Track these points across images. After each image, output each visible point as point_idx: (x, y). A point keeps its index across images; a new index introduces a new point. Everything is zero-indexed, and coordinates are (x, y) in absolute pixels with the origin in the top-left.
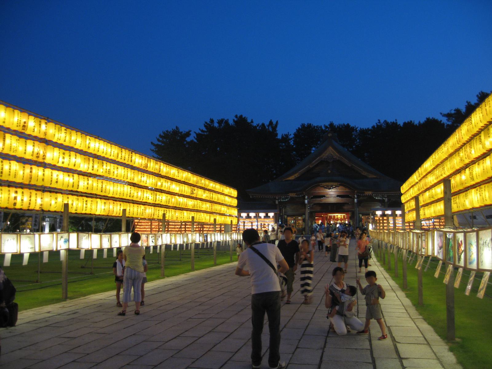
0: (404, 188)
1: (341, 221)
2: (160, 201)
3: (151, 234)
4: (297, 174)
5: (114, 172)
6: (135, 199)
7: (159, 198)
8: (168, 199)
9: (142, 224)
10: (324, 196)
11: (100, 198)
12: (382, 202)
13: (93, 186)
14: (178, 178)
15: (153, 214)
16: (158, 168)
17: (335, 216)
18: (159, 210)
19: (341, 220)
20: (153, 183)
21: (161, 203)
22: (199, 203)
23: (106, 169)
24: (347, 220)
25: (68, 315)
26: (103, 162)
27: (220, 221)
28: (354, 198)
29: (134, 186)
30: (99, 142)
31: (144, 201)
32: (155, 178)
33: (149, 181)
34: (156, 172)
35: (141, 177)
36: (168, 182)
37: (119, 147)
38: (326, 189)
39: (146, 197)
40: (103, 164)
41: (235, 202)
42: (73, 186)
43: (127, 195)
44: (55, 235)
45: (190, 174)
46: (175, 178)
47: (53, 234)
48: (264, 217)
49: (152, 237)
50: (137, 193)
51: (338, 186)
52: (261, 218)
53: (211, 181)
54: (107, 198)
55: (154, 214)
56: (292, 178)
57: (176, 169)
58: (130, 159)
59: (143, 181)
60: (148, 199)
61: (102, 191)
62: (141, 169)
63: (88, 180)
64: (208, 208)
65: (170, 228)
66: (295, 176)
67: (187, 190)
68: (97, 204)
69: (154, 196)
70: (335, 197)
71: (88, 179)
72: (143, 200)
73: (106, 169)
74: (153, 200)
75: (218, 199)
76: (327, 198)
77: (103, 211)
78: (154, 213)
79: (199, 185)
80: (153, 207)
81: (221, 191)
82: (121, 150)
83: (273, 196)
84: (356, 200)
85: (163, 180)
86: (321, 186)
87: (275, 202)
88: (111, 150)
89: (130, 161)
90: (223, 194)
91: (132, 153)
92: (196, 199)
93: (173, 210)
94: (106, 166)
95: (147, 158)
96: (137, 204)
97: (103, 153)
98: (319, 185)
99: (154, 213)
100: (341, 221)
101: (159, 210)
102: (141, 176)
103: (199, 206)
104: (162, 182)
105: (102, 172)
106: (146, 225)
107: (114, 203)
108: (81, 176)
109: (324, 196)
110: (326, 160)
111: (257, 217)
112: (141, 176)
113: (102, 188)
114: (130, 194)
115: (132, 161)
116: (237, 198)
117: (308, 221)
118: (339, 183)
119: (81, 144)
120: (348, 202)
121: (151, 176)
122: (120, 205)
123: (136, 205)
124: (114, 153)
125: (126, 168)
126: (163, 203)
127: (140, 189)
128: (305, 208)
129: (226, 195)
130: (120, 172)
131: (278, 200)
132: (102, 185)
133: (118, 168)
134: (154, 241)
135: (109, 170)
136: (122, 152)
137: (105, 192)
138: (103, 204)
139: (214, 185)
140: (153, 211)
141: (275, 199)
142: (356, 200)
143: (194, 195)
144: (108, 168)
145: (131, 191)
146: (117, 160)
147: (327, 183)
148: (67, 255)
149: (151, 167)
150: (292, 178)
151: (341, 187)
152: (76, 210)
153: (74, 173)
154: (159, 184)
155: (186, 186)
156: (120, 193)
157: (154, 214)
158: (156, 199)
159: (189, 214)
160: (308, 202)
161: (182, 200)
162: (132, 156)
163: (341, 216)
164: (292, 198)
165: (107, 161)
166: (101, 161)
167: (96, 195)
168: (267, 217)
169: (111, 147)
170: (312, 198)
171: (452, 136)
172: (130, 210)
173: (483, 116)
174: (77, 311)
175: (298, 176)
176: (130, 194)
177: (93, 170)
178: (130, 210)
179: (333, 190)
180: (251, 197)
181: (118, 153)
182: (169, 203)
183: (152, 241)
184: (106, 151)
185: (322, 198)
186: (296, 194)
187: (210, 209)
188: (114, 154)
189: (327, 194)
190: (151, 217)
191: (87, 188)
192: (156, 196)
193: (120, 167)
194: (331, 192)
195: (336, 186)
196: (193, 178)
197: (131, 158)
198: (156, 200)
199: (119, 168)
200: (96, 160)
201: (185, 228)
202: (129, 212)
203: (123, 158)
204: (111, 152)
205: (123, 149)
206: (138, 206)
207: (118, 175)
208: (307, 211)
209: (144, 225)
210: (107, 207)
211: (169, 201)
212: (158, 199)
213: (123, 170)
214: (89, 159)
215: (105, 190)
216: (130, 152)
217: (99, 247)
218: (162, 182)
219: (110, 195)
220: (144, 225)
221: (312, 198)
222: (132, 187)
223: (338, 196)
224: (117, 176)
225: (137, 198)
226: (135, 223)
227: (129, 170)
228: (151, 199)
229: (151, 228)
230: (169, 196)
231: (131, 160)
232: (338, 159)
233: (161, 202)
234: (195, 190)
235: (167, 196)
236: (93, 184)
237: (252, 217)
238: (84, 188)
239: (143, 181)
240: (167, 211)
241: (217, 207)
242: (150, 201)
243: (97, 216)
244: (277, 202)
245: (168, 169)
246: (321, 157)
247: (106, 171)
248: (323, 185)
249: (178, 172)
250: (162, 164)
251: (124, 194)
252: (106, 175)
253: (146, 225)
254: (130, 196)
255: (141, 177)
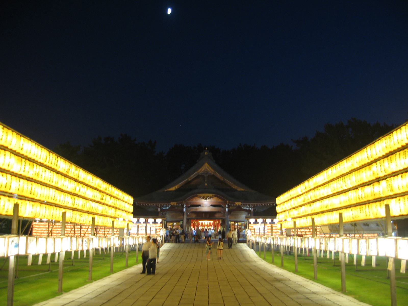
1: (208, 227)
2: (77, 205)
12: (249, 211)
33: (69, 185)
37: (48, 151)
39: (67, 201)
40: (33, 165)
41: (131, 209)
42: (6, 187)
44: (6, 238)
47: (5, 237)
51: (212, 197)
55: (72, 218)
56: (173, 189)
61: (31, 193)
66: (176, 188)
67: (97, 196)
70: (209, 206)
76: (202, 207)
78: (72, 216)
79: (107, 191)
82: (49, 154)
84: (227, 210)
91: (58, 157)
96: (59, 207)
98: (196, 196)
99: (72, 216)
100: (208, 227)
106: (44, 228)
108: (13, 177)
110: (202, 175)
111: (264, 222)
115: (9, 166)
117: (186, 227)
120: (220, 211)
123: (58, 208)
126: (79, 208)
128: (183, 215)
136: (50, 155)
142: (227, 210)
143: (103, 201)
144: (37, 170)
150: (173, 189)
151: (215, 198)
152: (7, 212)
153: (7, 174)
154: (77, 189)
156: (46, 196)
157: (72, 218)
160: (186, 210)
162: (57, 160)
164: (172, 207)
165: (37, 164)
168: (155, 222)
169: (41, 150)
170: (189, 207)
175: (179, 187)
180: (137, 204)
181: (46, 157)
182: (84, 207)
185: (198, 207)
189: (203, 204)
192: (75, 200)
195: (211, 197)
198: (74, 204)
200: (27, 161)
203: (50, 162)
205: (50, 153)
209: (42, 228)
211: (84, 206)
215: (34, 192)
216: (57, 156)
217: (44, 252)
218: (80, 188)
220: (42, 228)
223: (211, 206)
226: (33, 226)
229: (80, 231)
242: (70, 205)
244: (159, 210)
248: (200, 196)
249: (93, 179)
250: (81, 170)
253: (44, 228)
254: (54, 199)
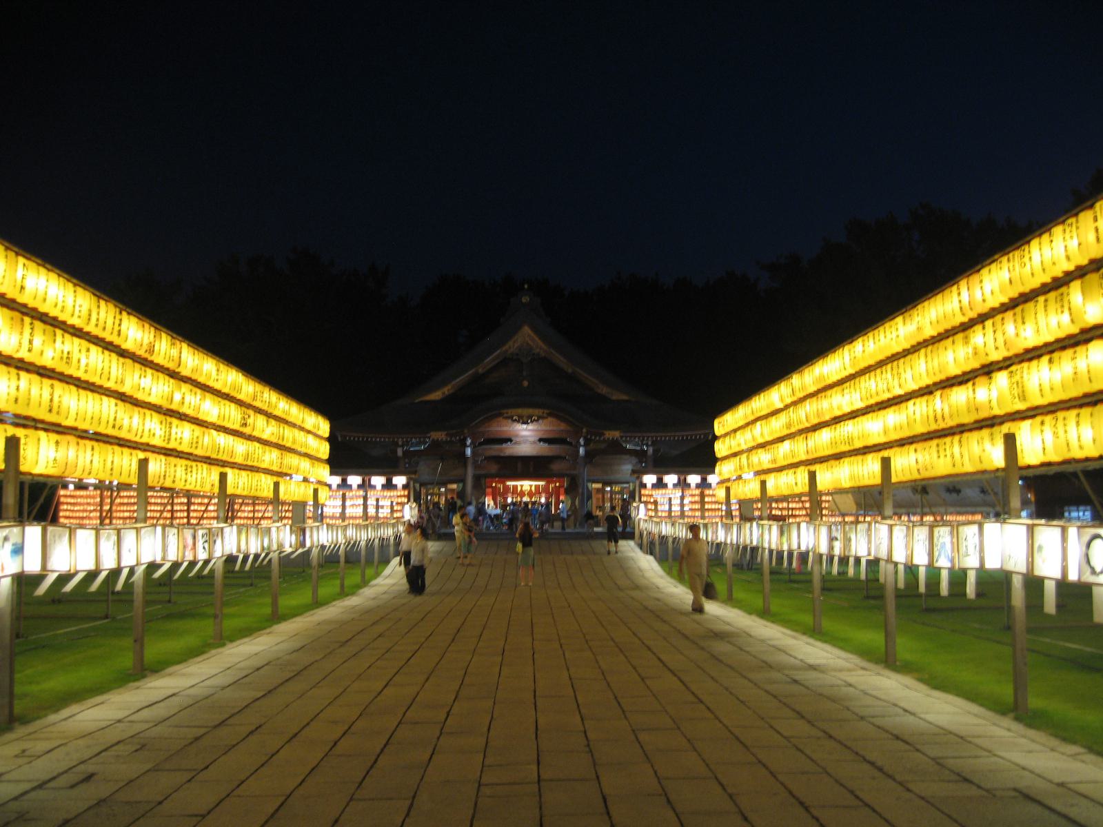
0: (721, 425)
1: (531, 498)
2: (179, 441)
3: (172, 525)
4: (449, 387)
5: (79, 361)
6: (123, 434)
7: (176, 433)
8: (195, 438)
9: (79, 500)
10: (510, 440)
11: (46, 430)
12: (640, 455)
13: (29, 394)
14: (217, 386)
15: (163, 474)
16: (175, 355)
17: (517, 486)
18: (175, 466)
19: (531, 494)
20: (166, 393)
21: (180, 448)
22: (257, 448)
23: (62, 352)
24: (543, 495)
25: (72, 787)
26: (54, 331)
27: (296, 495)
28: (577, 446)
29: (123, 401)
30: (47, 275)
31: (144, 440)
32: (169, 382)
33: (155, 388)
34: (171, 365)
35: (140, 378)
36: (195, 393)
37: (94, 295)
38: (515, 424)
41: (324, 450)
43: (108, 422)
45: (240, 374)
46: (211, 383)
48: (383, 486)
49: (203, 536)
50: (131, 418)
52: (374, 487)
53: (281, 397)
54: (60, 429)
55: (165, 476)
56: (436, 396)
57: (214, 362)
58: (117, 328)
59: (144, 389)
60: (154, 435)
61: (50, 411)
62: (139, 357)
63: (19, 379)
64: (275, 461)
65: (151, 511)
66: (444, 393)
68: (39, 444)
69: (166, 427)
71: (18, 375)
72: (141, 437)
73: (62, 352)
74: (163, 438)
75: (294, 441)
76: (516, 443)
77: (51, 464)
78: (165, 472)
79: (257, 404)
80: (163, 458)
81: (299, 423)
83: (420, 438)
84: (582, 451)
85: (185, 388)
86: (505, 415)
87: (396, 452)
88: (75, 301)
89: (116, 332)
90: (302, 429)
91: (121, 313)
92: (250, 438)
93: (205, 466)
94: (63, 343)
95: (153, 330)
96: (129, 447)
97: (56, 306)
98: (500, 415)
99: (165, 472)
100: (531, 498)
101: (175, 466)
102: (141, 375)
103: (256, 456)
104: (184, 394)
105: (53, 359)
106: (88, 504)
107: (78, 444)
109: (510, 440)
112: (141, 375)
113: (51, 400)
114: (115, 420)
116: (331, 439)
118: (545, 411)
119: (4, 277)
120: (563, 455)
121: (161, 375)
122: (93, 449)
123: (126, 451)
124: (82, 309)
125: (107, 353)
126: (185, 448)
127: (136, 409)
128: (465, 466)
129: (309, 432)
130: (92, 363)
131: (402, 446)
132: (52, 395)
133: (88, 350)
134: (206, 545)
135: (68, 353)
136: (99, 307)
137: (58, 413)
138: (53, 446)
139: (287, 407)
140: (163, 466)
141: (397, 445)
142: (582, 451)
143: (247, 430)
145: (116, 412)
146: (87, 329)
147: (520, 411)
148: (13, 593)
149: (161, 354)
150: (436, 396)
151: (550, 419)
154: (177, 397)
155: (233, 405)
156: (92, 418)
157: (165, 476)
158: (170, 435)
159: (237, 476)
160: (473, 452)
161: (224, 440)
162: (121, 320)
163: (531, 486)
164: (436, 444)
165: (65, 331)
166: (49, 328)
167: (35, 420)
168: (389, 486)
169: (75, 292)
170: (481, 444)
171: (939, 297)
172: (112, 462)
173: (1080, 244)
174: (90, 768)
175: (451, 392)
176: (115, 420)
177: (30, 350)
178: (112, 462)
179: (531, 427)
180: (340, 439)
181: (90, 311)
182: (196, 447)
183: (204, 548)
184: (63, 301)
185: (504, 445)
186: (446, 435)
187: (279, 464)
188: (80, 311)
189: (517, 436)
190: (158, 482)
191: (16, 400)
192: (171, 428)
193: (94, 348)
194: (526, 430)
195: (540, 418)
196: (246, 387)
197: (120, 325)
198: (169, 440)
199: (91, 350)
200: (38, 324)
201: (172, 511)
202: (112, 469)
204: (74, 306)
206: (131, 454)
207: (89, 369)
208: (470, 472)
210: (61, 454)
212: (173, 437)
213: (101, 357)
214: (22, 320)
215: (59, 407)
216: (118, 310)
218: (184, 394)
219: (69, 422)
221: (481, 444)
222: (120, 403)
223: (540, 440)
224: (86, 371)
225: (129, 431)
226: (58, 499)
227: (114, 356)
228: (160, 437)
230: (198, 430)
231: (119, 331)
232: (543, 355)
233: (180, 443)
234: (249, 416)
235: (193, 431)
236: (29, 390)
237: (355, 487)
238: (8, 400)
239: (144, 389)
240: (191, 467)
241: (293, 460)
242: (157, 441)
243: (36, 478)
244: (400, 452)
245: (197, 361)
246: (504, 349)
247: (60, 355)
248: (509, 414)
249: (218, 370)
250: (185, 346)
251: (102, 420)
252: (61, 367)
253: (88, 504)
254: (114, 427)
255: (140, 378)
